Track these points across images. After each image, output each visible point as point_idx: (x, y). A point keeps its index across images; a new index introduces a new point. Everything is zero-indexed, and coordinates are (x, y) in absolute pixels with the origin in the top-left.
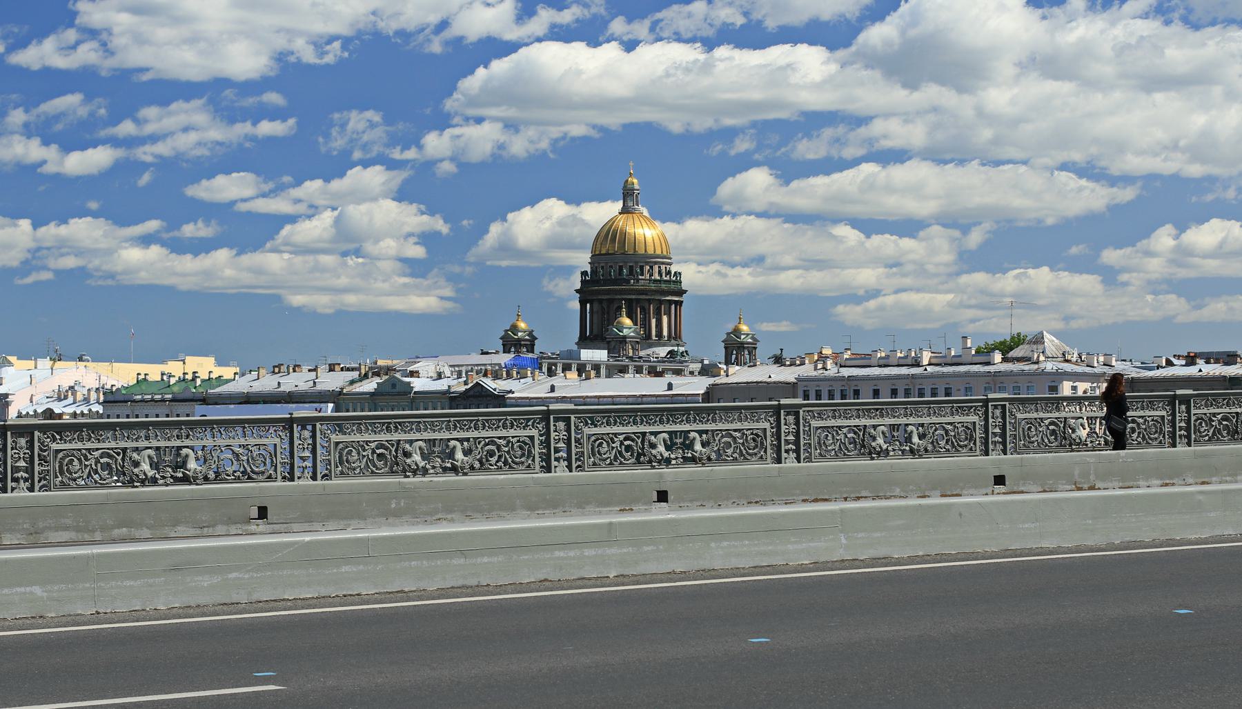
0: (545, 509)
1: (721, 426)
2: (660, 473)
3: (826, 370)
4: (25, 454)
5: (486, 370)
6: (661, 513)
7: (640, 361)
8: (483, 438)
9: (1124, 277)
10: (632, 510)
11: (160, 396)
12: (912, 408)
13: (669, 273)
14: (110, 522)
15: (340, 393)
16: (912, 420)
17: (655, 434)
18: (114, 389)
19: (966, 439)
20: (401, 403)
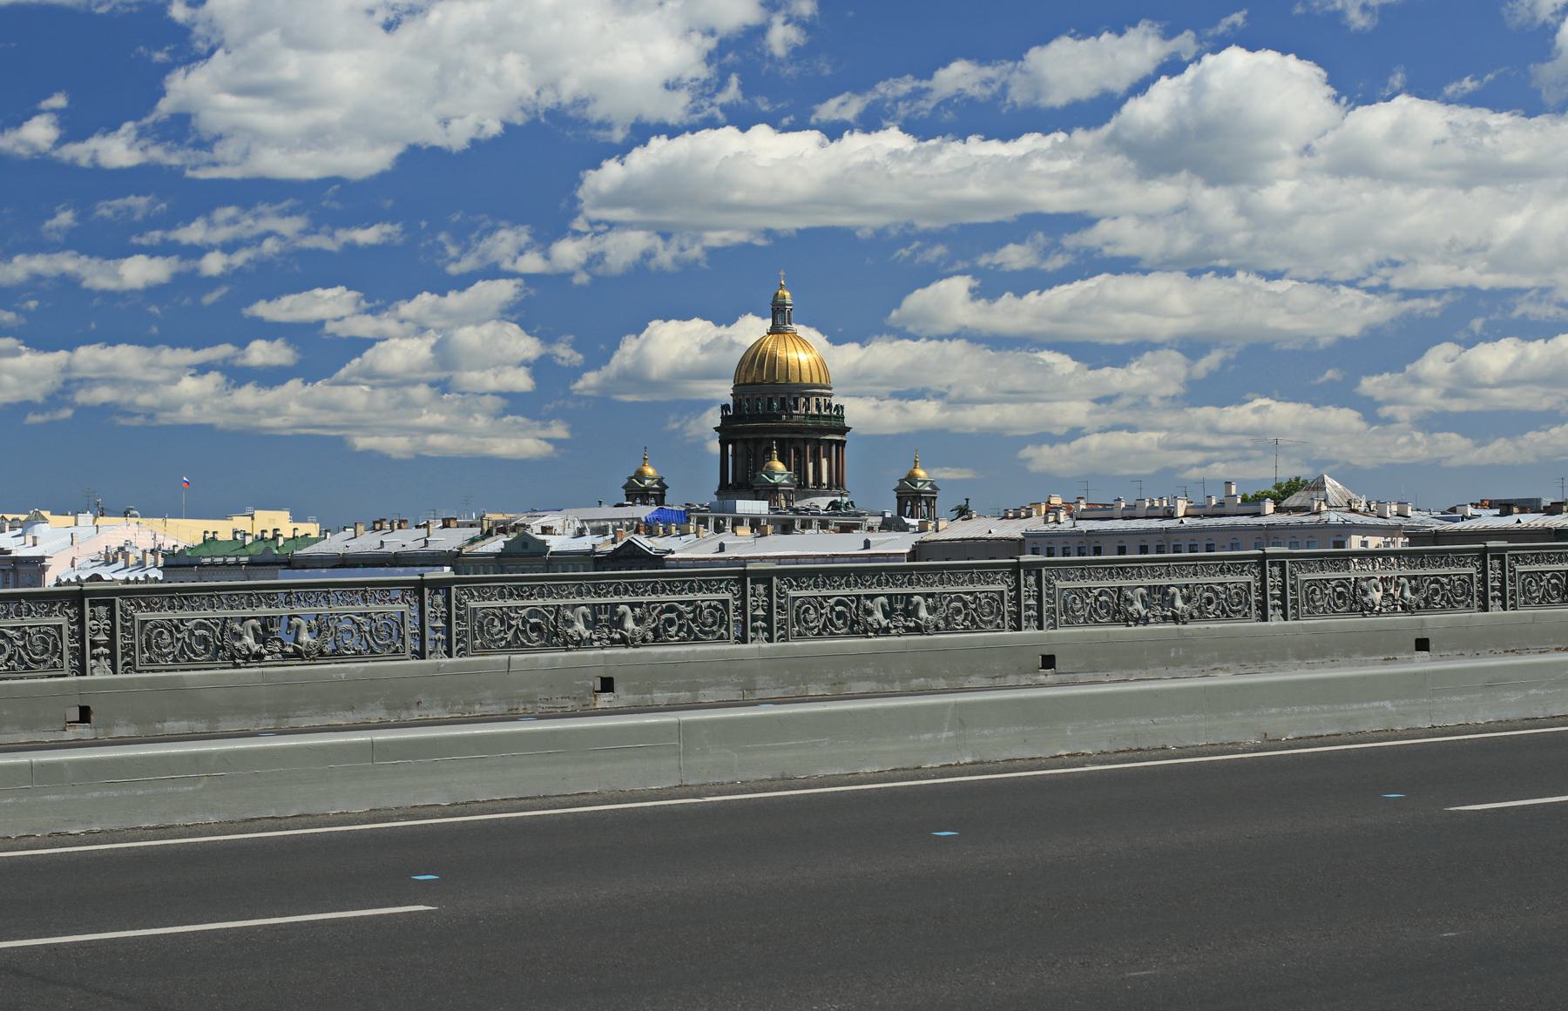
0: (1315, 658)
1: (1429, 571)
2: (1422, 620)
3: (1059, 523)
4: (763, 601)
5: (638, 526)
6: (1422, 664)
7: (807, 515)
8: (948, 593)
9: (1386, 411)
10: (1395, 659)
11: (234, 559)
12: (1178, 566)
13: (829, 406)
14: (908, 672)
15: (459, 554)
16: (1175, 581)
17: (871, 597)
18: (177, 550)
19: (992, 613)
20: (521, 567)
